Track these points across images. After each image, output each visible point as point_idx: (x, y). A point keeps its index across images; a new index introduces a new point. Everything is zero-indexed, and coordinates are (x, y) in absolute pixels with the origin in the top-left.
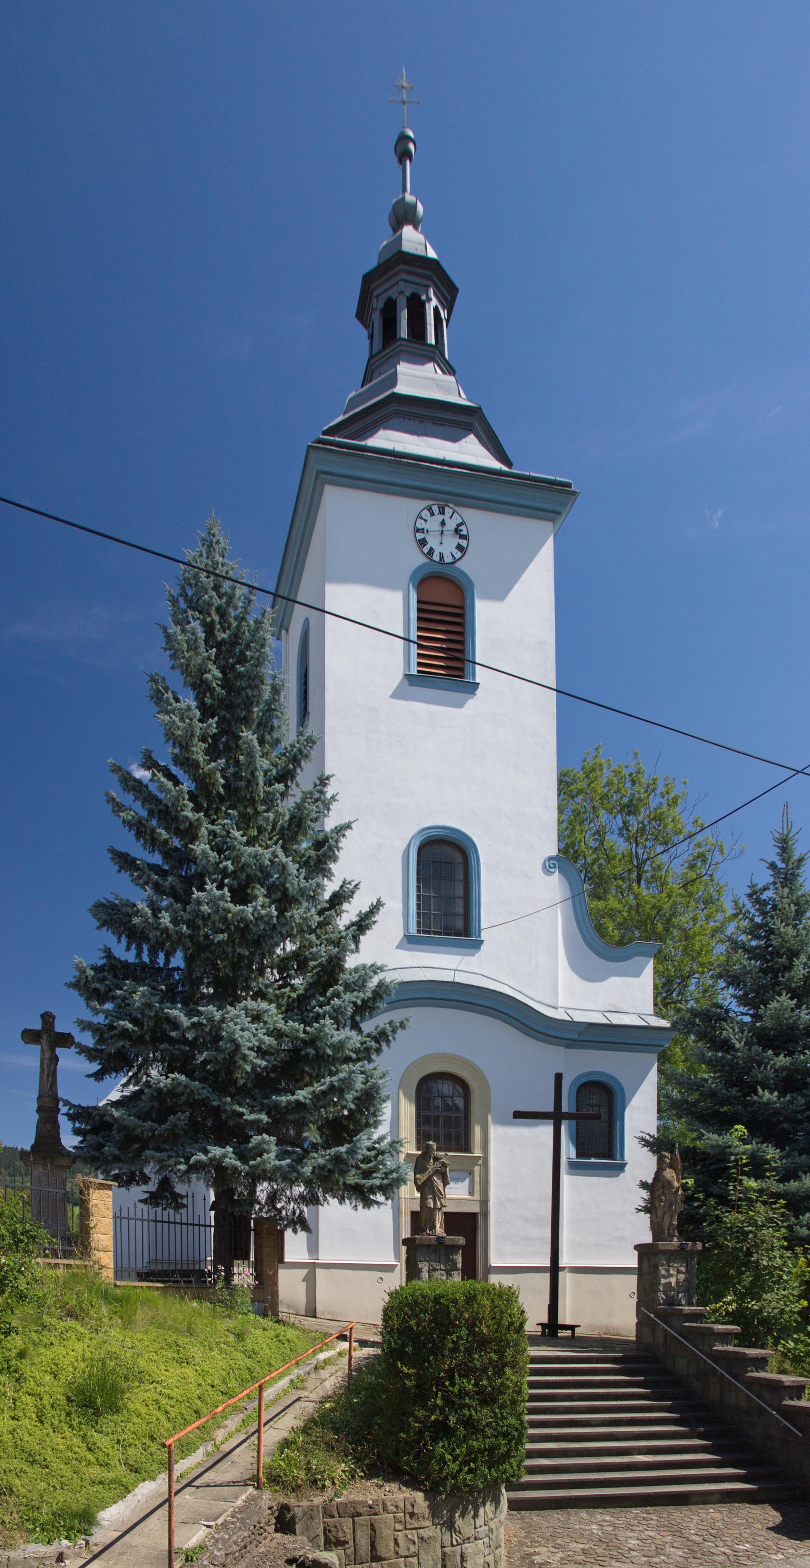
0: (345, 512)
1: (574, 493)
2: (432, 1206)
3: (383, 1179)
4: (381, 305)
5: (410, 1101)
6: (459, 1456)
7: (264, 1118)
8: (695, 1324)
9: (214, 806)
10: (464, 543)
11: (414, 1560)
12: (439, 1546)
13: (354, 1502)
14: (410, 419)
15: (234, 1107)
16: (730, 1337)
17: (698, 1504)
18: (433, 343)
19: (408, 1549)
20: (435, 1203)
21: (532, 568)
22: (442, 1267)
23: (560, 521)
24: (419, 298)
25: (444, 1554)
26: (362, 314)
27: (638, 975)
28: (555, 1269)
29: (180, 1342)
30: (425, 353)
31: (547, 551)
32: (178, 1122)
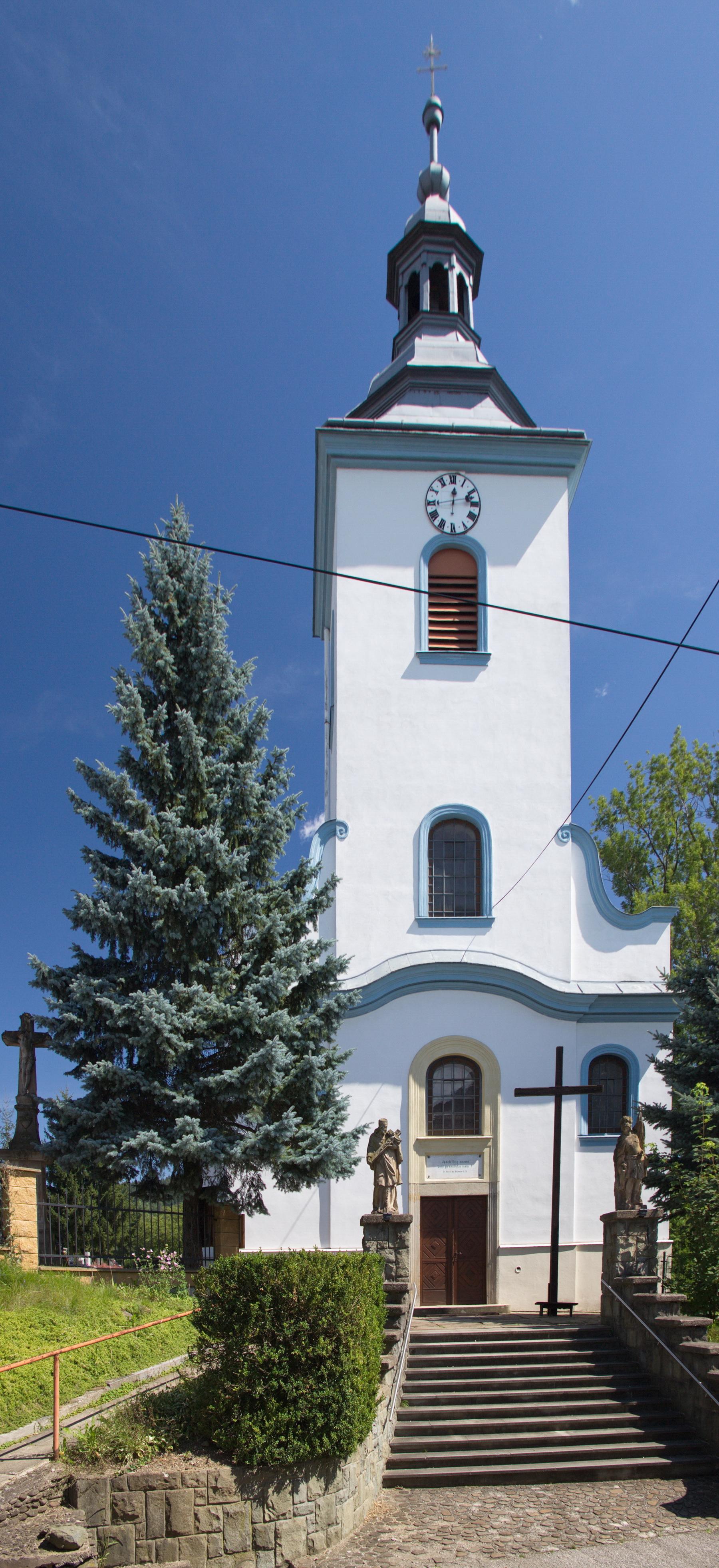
1: (586, 443)
2: (383, 1184)
5: (420, 1086)
6: (268, 1429)
7: (191, 1099)
8: (647, 1294)
9: (168, 793)
10: (475, 510)
11: (219, 1536)
12: (248, 1521)
13: (148, 1475)
14: (425, 391)
15: (163, 1091)
16: (675, 1306)
17: (606, 1480)
18: (456, 310)
19: (211, 1525)
20: (387, 1181)
23: (576, 475)
25: (254, 1530)
26: (392, 297)
27: (654, 941)
28: (555, 1249)
29: (56, 1320)
31: (562, 507)
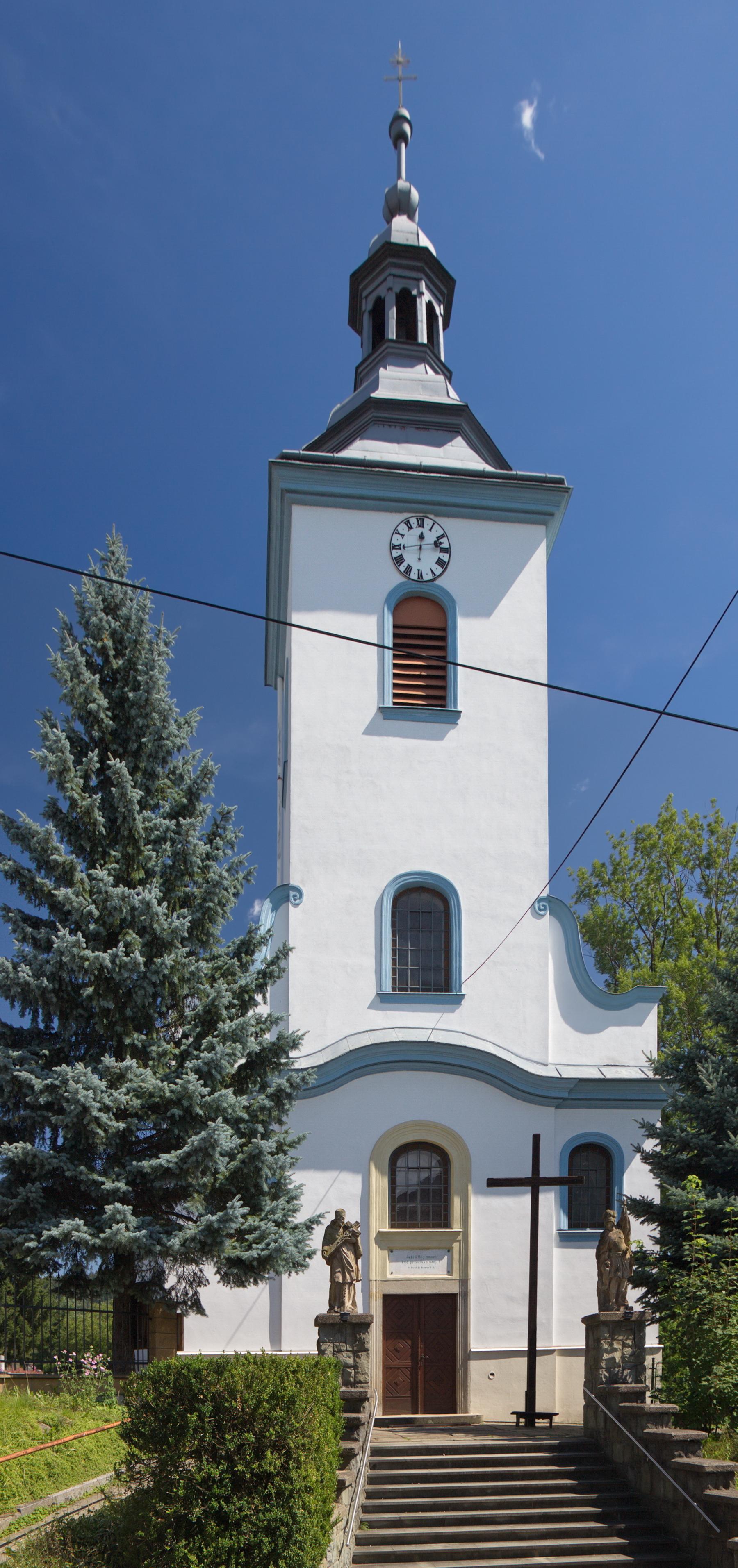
0: (319, 535)
1: (567, 490)
2: (341, 1280)
3: (263, 1250)
4: (370, 306)
5: (382, 1174)
6: (206, 1557)
7: (122, 1185)
8: (635, 1404)
10: (445, 557)
14: (390, 426)
18: (425, 341)
21: (521, 578)
22: (349, 1348)
24: (410, 292)
26: (354, 321)
27: (640, 1023)
28: (532, 1354)
30: (413, 353)
31: (539, 559)
32: (29, 1195)
